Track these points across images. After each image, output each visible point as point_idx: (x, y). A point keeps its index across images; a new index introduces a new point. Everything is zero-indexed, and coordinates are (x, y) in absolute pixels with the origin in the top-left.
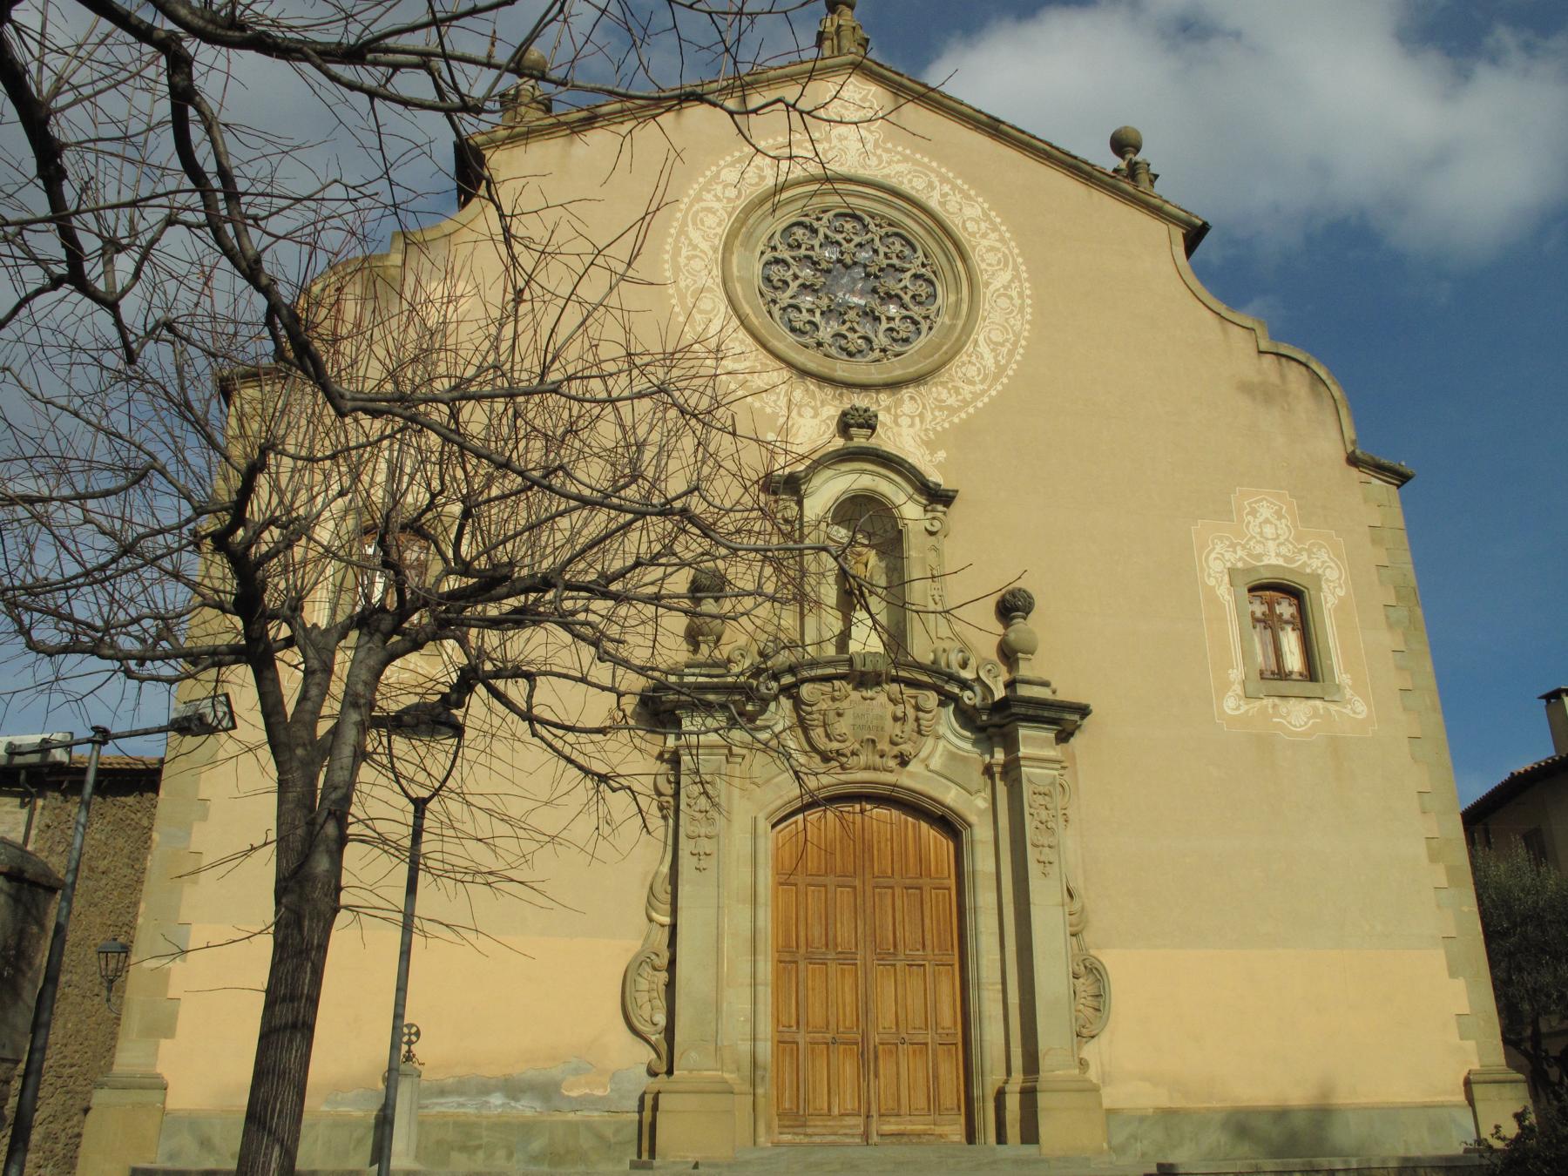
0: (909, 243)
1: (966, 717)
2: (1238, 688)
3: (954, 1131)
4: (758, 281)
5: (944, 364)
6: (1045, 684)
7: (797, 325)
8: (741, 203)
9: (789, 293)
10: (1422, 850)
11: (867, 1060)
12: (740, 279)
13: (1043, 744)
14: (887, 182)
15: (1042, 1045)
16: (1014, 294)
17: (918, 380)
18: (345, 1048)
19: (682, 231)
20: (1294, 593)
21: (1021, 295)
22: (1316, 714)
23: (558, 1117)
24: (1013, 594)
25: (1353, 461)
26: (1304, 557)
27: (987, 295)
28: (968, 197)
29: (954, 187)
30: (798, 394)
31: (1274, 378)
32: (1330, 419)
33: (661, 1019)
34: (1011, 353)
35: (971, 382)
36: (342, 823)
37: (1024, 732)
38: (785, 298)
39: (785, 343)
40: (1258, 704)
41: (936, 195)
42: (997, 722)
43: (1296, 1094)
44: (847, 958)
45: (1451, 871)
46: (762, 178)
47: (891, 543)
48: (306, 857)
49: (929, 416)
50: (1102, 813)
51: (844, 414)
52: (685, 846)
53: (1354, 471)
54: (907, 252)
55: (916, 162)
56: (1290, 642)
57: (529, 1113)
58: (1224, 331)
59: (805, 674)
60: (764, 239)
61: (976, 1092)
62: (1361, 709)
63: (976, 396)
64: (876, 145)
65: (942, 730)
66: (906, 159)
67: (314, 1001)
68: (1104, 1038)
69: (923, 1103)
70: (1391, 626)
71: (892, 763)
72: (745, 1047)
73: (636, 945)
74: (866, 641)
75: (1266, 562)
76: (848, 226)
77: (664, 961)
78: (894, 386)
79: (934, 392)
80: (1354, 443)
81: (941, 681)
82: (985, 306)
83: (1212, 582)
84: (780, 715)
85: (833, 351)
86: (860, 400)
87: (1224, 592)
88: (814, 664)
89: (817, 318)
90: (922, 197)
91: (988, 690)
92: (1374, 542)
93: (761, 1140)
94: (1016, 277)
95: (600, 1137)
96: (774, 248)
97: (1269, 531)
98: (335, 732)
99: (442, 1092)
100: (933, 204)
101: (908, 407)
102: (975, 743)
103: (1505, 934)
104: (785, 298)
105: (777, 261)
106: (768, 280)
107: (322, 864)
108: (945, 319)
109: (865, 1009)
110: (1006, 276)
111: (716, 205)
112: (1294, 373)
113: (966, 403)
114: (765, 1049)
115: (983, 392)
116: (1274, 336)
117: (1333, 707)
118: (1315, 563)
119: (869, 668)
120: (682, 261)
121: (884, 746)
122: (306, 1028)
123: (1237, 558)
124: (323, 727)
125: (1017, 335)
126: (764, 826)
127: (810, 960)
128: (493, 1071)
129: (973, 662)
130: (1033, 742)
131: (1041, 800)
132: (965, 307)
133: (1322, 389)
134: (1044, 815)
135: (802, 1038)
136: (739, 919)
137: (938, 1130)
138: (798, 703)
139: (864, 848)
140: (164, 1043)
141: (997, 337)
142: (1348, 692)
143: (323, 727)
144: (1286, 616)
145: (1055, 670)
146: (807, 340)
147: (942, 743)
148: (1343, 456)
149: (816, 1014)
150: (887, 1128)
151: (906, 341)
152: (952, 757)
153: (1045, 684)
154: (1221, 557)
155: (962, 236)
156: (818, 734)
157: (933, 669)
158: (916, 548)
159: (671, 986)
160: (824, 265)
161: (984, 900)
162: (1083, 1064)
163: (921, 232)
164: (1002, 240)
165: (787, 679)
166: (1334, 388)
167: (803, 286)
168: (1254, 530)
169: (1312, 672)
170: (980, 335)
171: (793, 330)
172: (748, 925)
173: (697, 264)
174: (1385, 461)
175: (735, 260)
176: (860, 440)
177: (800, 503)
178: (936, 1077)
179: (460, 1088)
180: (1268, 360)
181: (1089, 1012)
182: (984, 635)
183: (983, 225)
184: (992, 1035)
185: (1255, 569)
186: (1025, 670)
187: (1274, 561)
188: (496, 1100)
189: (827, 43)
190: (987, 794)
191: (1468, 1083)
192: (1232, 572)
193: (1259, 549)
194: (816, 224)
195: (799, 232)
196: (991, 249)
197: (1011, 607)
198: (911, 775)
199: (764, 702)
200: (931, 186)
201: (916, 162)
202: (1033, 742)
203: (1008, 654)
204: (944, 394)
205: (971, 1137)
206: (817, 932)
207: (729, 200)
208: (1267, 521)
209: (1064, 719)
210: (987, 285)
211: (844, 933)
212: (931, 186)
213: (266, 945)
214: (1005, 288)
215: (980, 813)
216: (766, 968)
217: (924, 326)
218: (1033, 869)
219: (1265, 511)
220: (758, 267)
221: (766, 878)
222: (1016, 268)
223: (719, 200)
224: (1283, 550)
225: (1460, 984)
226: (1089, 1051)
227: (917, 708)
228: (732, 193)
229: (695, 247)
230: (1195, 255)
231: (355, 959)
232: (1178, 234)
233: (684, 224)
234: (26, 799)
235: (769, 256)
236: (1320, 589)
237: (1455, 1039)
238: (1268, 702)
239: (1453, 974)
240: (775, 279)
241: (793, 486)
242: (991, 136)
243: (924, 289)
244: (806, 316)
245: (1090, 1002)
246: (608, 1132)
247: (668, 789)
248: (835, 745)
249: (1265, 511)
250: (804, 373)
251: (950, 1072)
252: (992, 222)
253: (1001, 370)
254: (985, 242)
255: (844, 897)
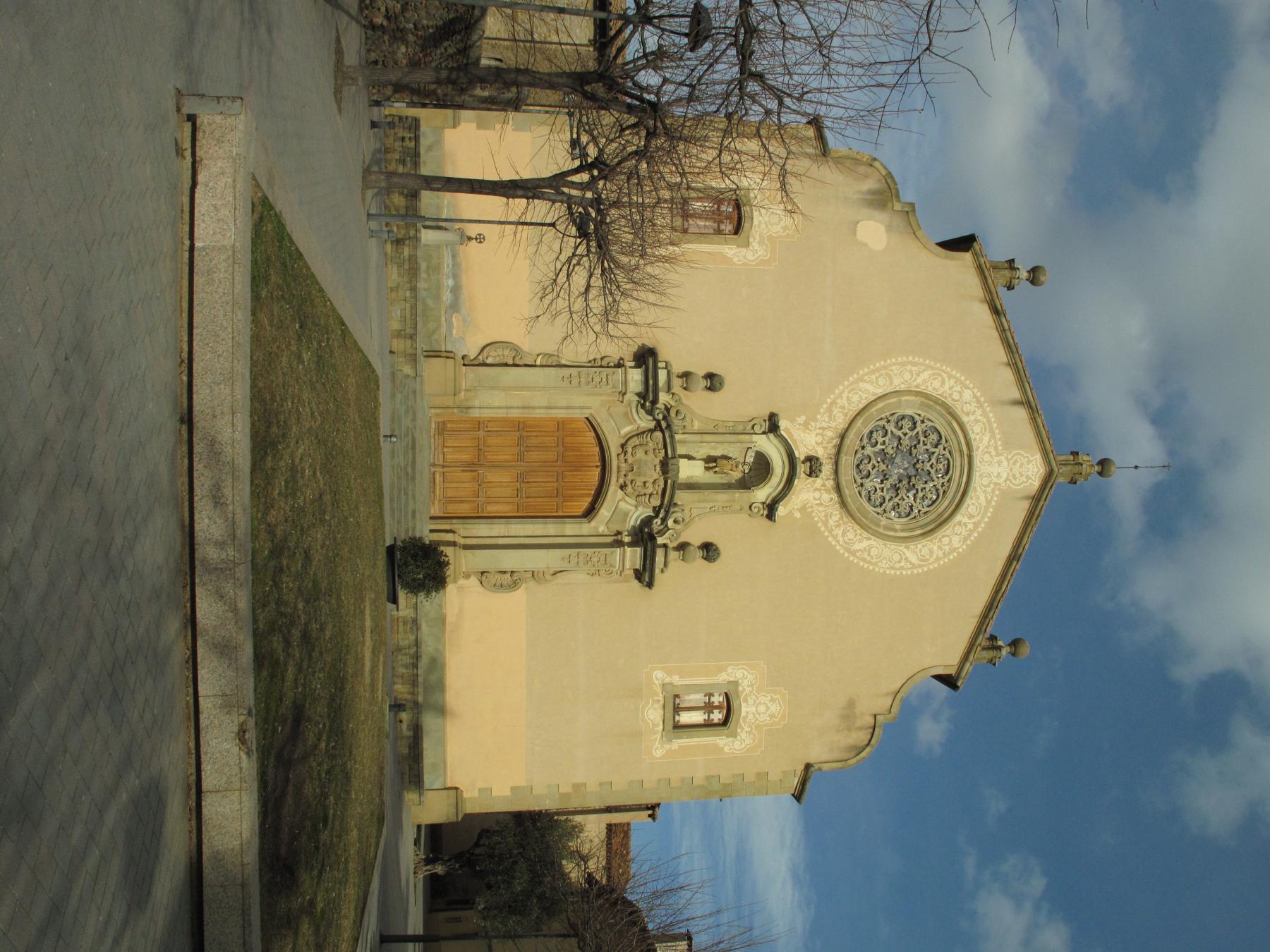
0: (934, 502)
1: (648, 521)
2: (668, 680)
3: (435, 511)
4: (901, 412)
5: (851, 516)
6: (666, 564)
7: (875, 434)
8: (949, 402)
9: (895, 431)
10: (579, 780)
11: (470, 466)
12: (900, 401)
13: (633, 562)
14: (971, 488)
15: (477, 552)
16: (902, 564)
17: (843, 504)
18: (470, 205)
19: (928, 367)
20: (725, 722)
21: (902, 568)
22: (655, 725)
23: (443, 312)
24: (717, 549)
25: (808, 766)
26: (747, 729)
27: (901, 547)
28: (965, 539)
29: (971, 531)
30: (829, 434)
31: (859, 723)
32: (836, 756)
33: (490, 361)
34: (864, 560)
35: (844, 534)
36: (533, 198)
37: (639, 550)
38: (891, 428)
39: (862, 427)
40: (659, 690)
41: (965, 520)
42: (644, 537)
43: (453, 697)
44: (521, 457)
45: (565, 796)
46: (967, 414)
47: (745, 484)
48: (522, 188)
49: (821, 509)
50: (595, 594)
51: (817, 459)
52: (574, 371)
53: (802, 767)
54: (927, 502)
55: (986, 509)
56: (697, 717)
57: (444, 298)
58: (888, 694)
59: (667, 435)
60: (929, 416)
61: (455, 521)
62: (658, 753)
63: (835, 537)
64: (996, 484)
65: (640, 509)
66: (989, 502)
67: (480, 193)
68: (481, 589)
69: (449, 495)
70: (708, 778)
71: (621, 481)
72: (477, 404)
73: (526, 348)
74: (689, 470)
75: (743, 705)
76: (941, 466)
77: (518, 362)
78: (838, 489)
79: (836, 514)
80: (820, 769)
81: (665, 508)
82: (893, 546)
83: (730, 670)
84: (645, 422)
85: (859, 455)
86: (827, 469)
87: (723, 678)
88: (672, 437)
89: (879, 447)
90: (963, 510)
91: (661, 533)
92: (758, 774)
93: (433, 411)
94: (914, 566)
95: (433, 333)
96: (923, 422)
97: (762, 709)
98: (563, 193)
99: (454, 256)
100: (958, 517)
101: (826, 497)
102: (633, 527)
103: (534, 824)
104: (891, 428)
105: (915, 423)
106: (903, 418)
107: (520, 192)
108: (884, 522)
109: (496, 466)
110: (914, 559)
111: (947, 386)
112: (863, 737)
113: (830, 531)
114: (475, 413)
115: (838, 542)
116: (887, 726)
117: (659, 736)
118: (744, 735)
119: (671, 467)
120: (909, 367)
121: (630, 476)
122: (473, 191)
123: (745, 687)
124: (566, 190)
125: (875, 564)
126: (587, 413)
127: (521, 437)
128: (464, 281)
129: (678, 527)
130: (633, 556)
131: (603, 558)
132: (892, 533)
133: (854, 753)
134: (595, 559)
135: (481, 433)
136: (539, 399)
137: (436, 502)
138: (652, 431)
139: (578, 467)
140: (474, 125)
141: (874, 552)
142: (668, 746)
143: (566, 190)
144: (712, 716)
145: (674, 574)
146: (865, 441)
147: (633, 509)
148: (811, 761)
149: (492, 441)
150: (437, 476)
151: (869, 499)
152: (626, 514)
153: (666, 564)
154: (744, 677)
155: (939, 534)
156: (635, 441)
157: (672, 504)
158: (740, 496)
159: (506, 365)
160: (914, 451)
161: (551, 528)
162: (467, 576)
163: (940, 510)
164: (938, 559)
165: (664, 424)
166: (854, 760)
167: (900, 439)
168: (762, 699)
169: (677, 726)
170: (874, 542)
171: (871, 432)
172: (536, 404)
173: (907, 376)
174: (808, 785)
175: (912, 398)
176: (802, 469)
177: (764, 433)
178: (462, 502)
179: (456, 265)
180: (871, 721)
181: (494, 581)
182: (695, 536)
183: (947, 548)
184: (483, 530)
185: (738, 697)
186: (673, 555)
187: (744, 710)
188: (451, 282)
189: (1071, 458)
190: (606, 532)
191: (456, 788)
192: (736, 683)
193: (751, 701)
194: (941, 447)
195: (934, 437)
196: (931, 551)
197: (709, 550)
198: (616, 492)
199: (650, 412)
200: (971, 517)
201: (986, 509)
202: (633, 556)
203: (683, 547)
204: (835, 518)
205: (432, 518)
206: (534, 441)
207: (951, 395)
208: (768, 708)
209: (645, 575)
210: (907, 548)
211: (534, 456)
212: (971, 517)
213: (497, 179)
214: (906, 559)
215: (596, 528)
216: (515, 414)
217: (879, 510)
218: (566, 552)
219: (774, 708)
220: (909, 412)
221: (561, 414)
222: (920, 566)
223: (950, 388)
224: (750, 716)
225: (507, 792)
226: (474, 581)
227: (651, 495)
228: (956, 396)
229: (918, 375)
230: (935, 681)
231: (492, 205)
232: (952, 671)
233: (932, 368)
234: (593, 42)
235: (917, 418)
236: (728, 736)
237: (480, 785)
238: (661, 698)
239: (513, 789)
240: (903, 422)
241: (773, 426)
242: (1009, 557)
243: (904, 509)
244: (880, 440)
245: (499, 582)
246: (435, 337)
247: (604, 363)
248: (630, 450)
249: (774, 708)
250: (843, 437)
251: (464, 509)
252: (949, 553)
253: (853, 553)
254: (935, 548)
255: (552, 456)
